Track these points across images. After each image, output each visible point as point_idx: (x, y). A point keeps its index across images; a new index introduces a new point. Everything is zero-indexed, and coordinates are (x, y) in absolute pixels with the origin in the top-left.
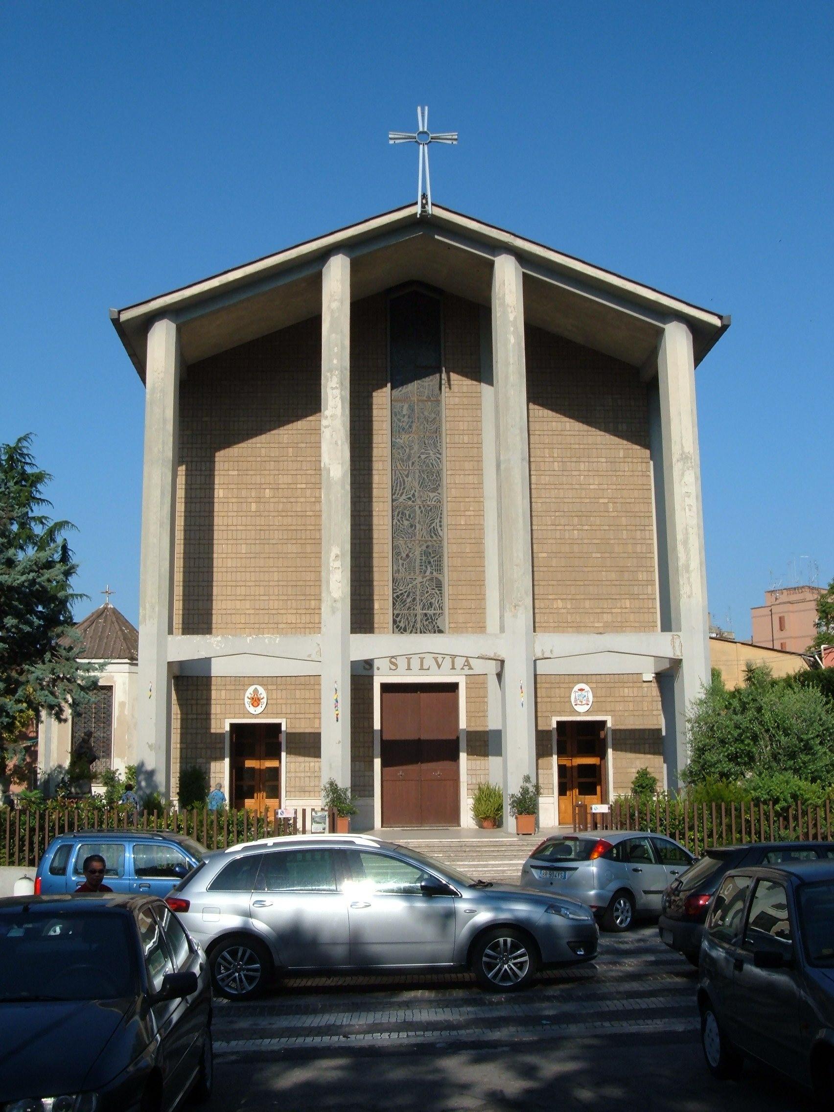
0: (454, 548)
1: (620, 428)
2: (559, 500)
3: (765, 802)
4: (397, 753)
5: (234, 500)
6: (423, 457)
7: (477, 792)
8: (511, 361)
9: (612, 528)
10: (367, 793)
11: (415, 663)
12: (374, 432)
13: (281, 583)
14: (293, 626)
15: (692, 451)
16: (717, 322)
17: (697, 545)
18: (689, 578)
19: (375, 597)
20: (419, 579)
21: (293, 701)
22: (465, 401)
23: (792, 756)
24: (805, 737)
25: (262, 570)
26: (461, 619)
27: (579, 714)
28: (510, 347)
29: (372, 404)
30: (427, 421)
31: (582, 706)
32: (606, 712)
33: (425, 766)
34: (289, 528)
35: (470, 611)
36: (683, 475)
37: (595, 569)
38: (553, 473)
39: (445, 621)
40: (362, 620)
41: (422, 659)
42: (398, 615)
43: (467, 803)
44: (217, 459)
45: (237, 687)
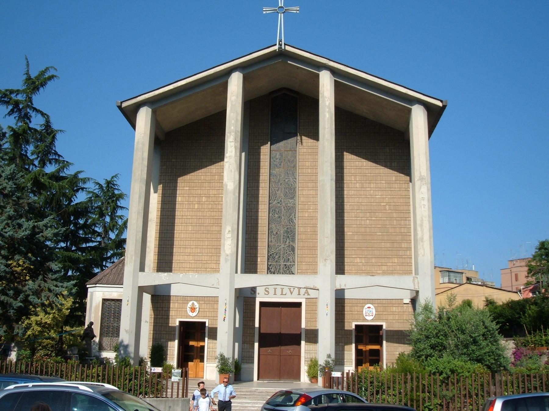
0: (302, 229)
1: (393, 165)
2: (359, 204)
3: (434, 374)
4: (267, 340)
5: (186, 203)
6: (286, 180)
7: (309, 362)
8: (327, 127)
9: (388, 219)
10: (250, 361)
11: (279, 291)
12: (261, 167)
13: (209, 247)
14: (214, 270)
15: (425, 175)
16: (439, 104)
17: (428, 227)
18: (423, 245)
19: (259, 255)
20: (283, 246)
21: (212, 310)
22: (310, 151)
23: (466, 346)
24: (473, 335)
25: (199, 239)
26: (304, 267)
27: (367, 321)
28: (326, 119)
29: (260, 153)
30: (289, 161)
31: (369, 316)
32: (383, 320)
33: (283, 348)
34: (215, 217)
35: (309, 263)
36: (420, 188)
37: (378, 241)
38: (355, 189)
39: (295, 269)
40: (250, 265)
41: (282, 289)
42: (271, 265)
43: (304, 368)
44: (178, 181)
45: (184, 302)
